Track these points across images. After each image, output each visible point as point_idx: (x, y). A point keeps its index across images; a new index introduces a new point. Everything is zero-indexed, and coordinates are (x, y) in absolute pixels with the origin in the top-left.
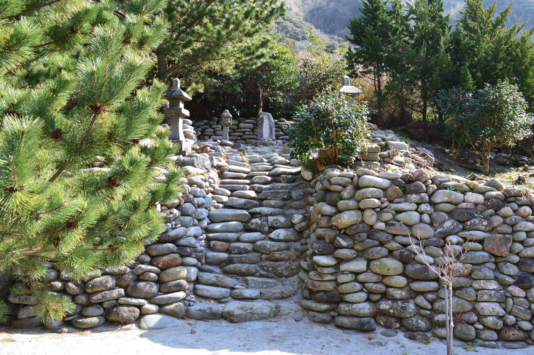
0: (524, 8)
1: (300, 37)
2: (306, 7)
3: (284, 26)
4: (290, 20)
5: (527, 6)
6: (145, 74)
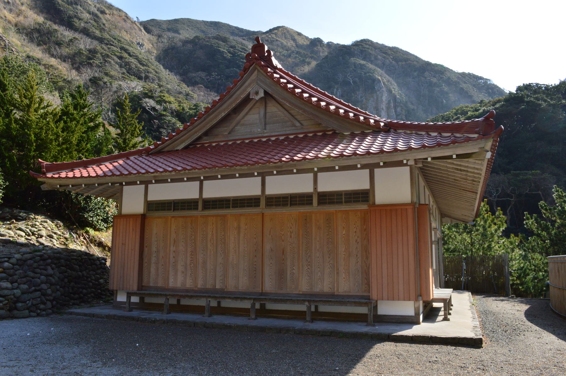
0: (365, 73)
1: (143, 75)
2: (161, 45)
3: (127, 62)
4: (136, 56)
5: (368, 73)
6: (354, 370)
